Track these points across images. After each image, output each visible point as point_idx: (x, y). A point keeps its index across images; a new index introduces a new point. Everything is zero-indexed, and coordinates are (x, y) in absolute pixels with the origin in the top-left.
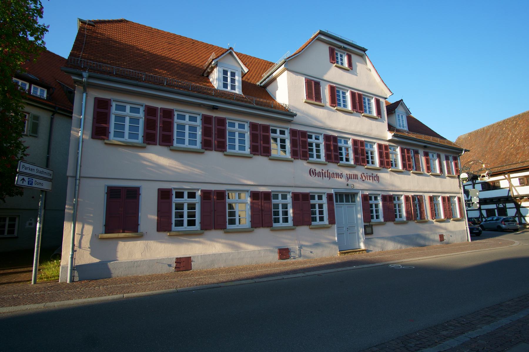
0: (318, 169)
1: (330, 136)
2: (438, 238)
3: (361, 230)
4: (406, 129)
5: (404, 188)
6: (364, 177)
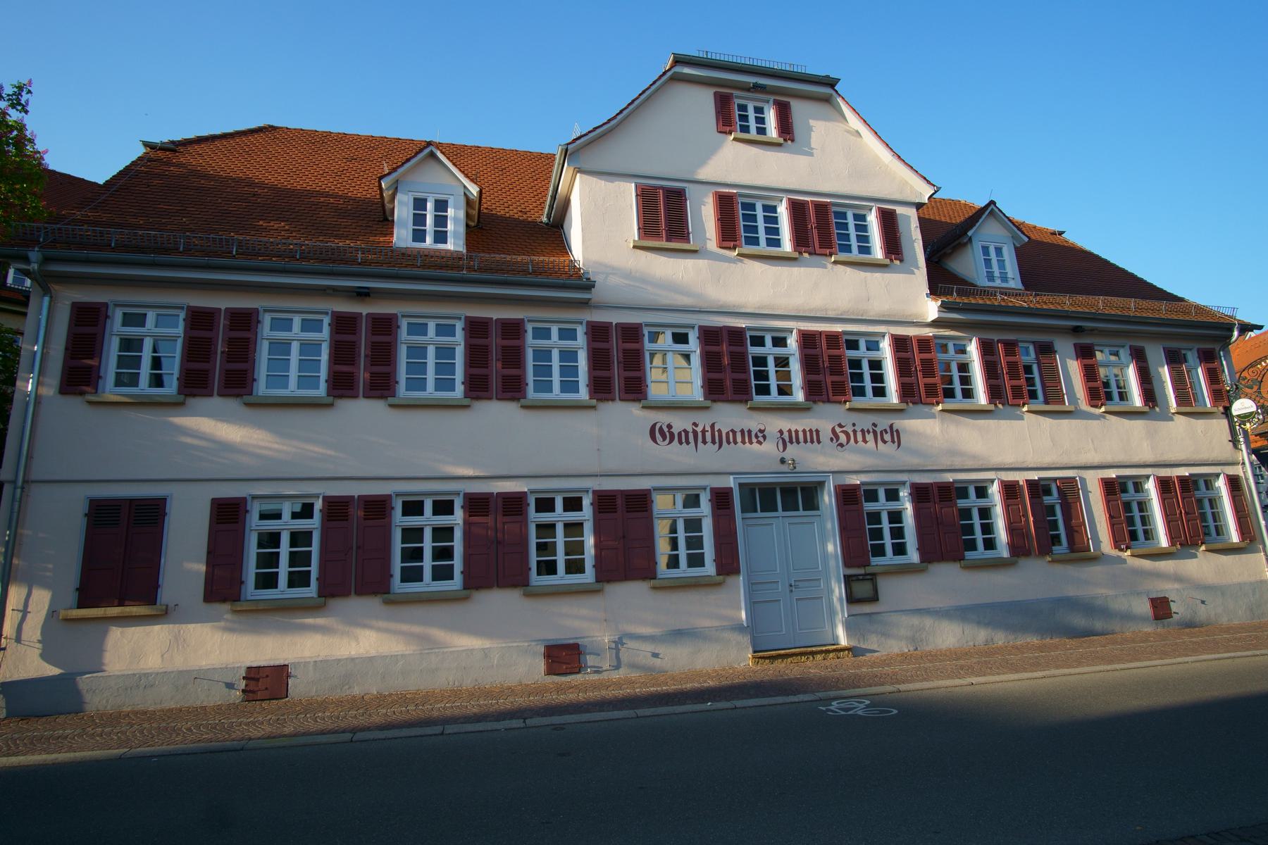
0: (680, 422)
1: (721, 329)
2: (1144, 608)
3: (838, 591)
4: (1015, 283)
5: (997, 460)
6: (843, 438)
